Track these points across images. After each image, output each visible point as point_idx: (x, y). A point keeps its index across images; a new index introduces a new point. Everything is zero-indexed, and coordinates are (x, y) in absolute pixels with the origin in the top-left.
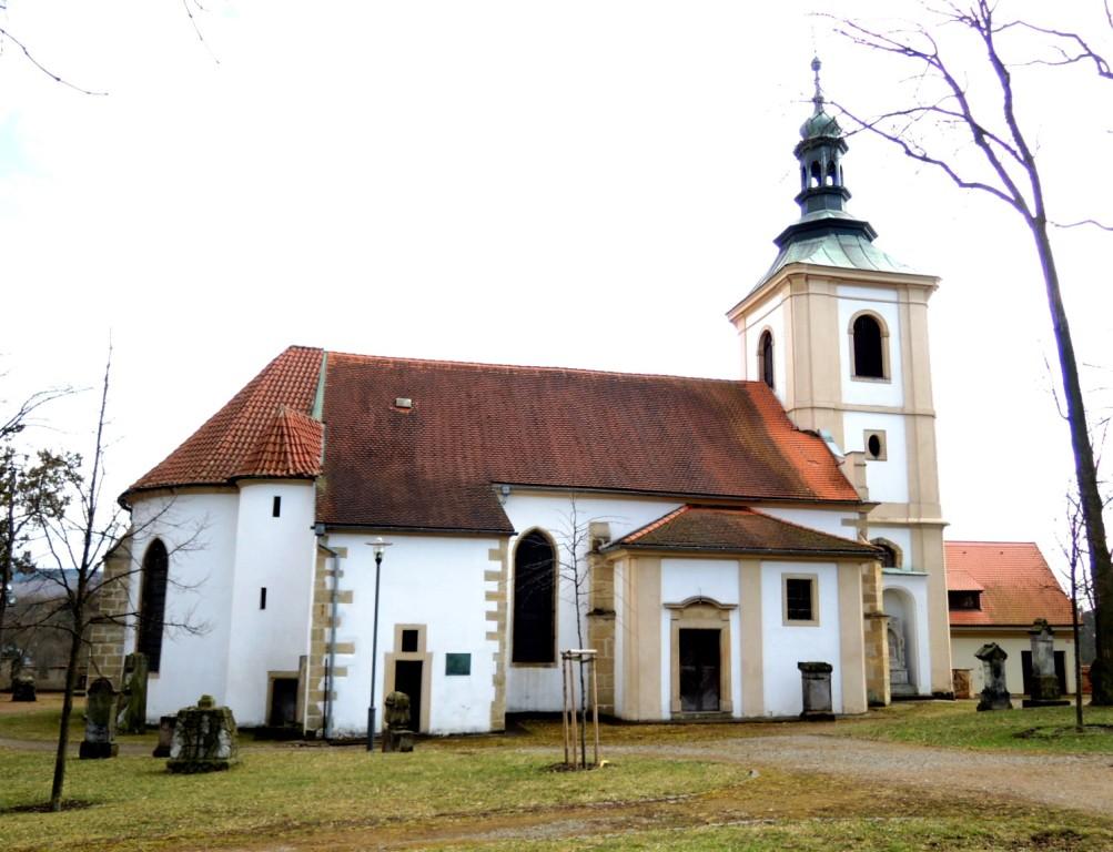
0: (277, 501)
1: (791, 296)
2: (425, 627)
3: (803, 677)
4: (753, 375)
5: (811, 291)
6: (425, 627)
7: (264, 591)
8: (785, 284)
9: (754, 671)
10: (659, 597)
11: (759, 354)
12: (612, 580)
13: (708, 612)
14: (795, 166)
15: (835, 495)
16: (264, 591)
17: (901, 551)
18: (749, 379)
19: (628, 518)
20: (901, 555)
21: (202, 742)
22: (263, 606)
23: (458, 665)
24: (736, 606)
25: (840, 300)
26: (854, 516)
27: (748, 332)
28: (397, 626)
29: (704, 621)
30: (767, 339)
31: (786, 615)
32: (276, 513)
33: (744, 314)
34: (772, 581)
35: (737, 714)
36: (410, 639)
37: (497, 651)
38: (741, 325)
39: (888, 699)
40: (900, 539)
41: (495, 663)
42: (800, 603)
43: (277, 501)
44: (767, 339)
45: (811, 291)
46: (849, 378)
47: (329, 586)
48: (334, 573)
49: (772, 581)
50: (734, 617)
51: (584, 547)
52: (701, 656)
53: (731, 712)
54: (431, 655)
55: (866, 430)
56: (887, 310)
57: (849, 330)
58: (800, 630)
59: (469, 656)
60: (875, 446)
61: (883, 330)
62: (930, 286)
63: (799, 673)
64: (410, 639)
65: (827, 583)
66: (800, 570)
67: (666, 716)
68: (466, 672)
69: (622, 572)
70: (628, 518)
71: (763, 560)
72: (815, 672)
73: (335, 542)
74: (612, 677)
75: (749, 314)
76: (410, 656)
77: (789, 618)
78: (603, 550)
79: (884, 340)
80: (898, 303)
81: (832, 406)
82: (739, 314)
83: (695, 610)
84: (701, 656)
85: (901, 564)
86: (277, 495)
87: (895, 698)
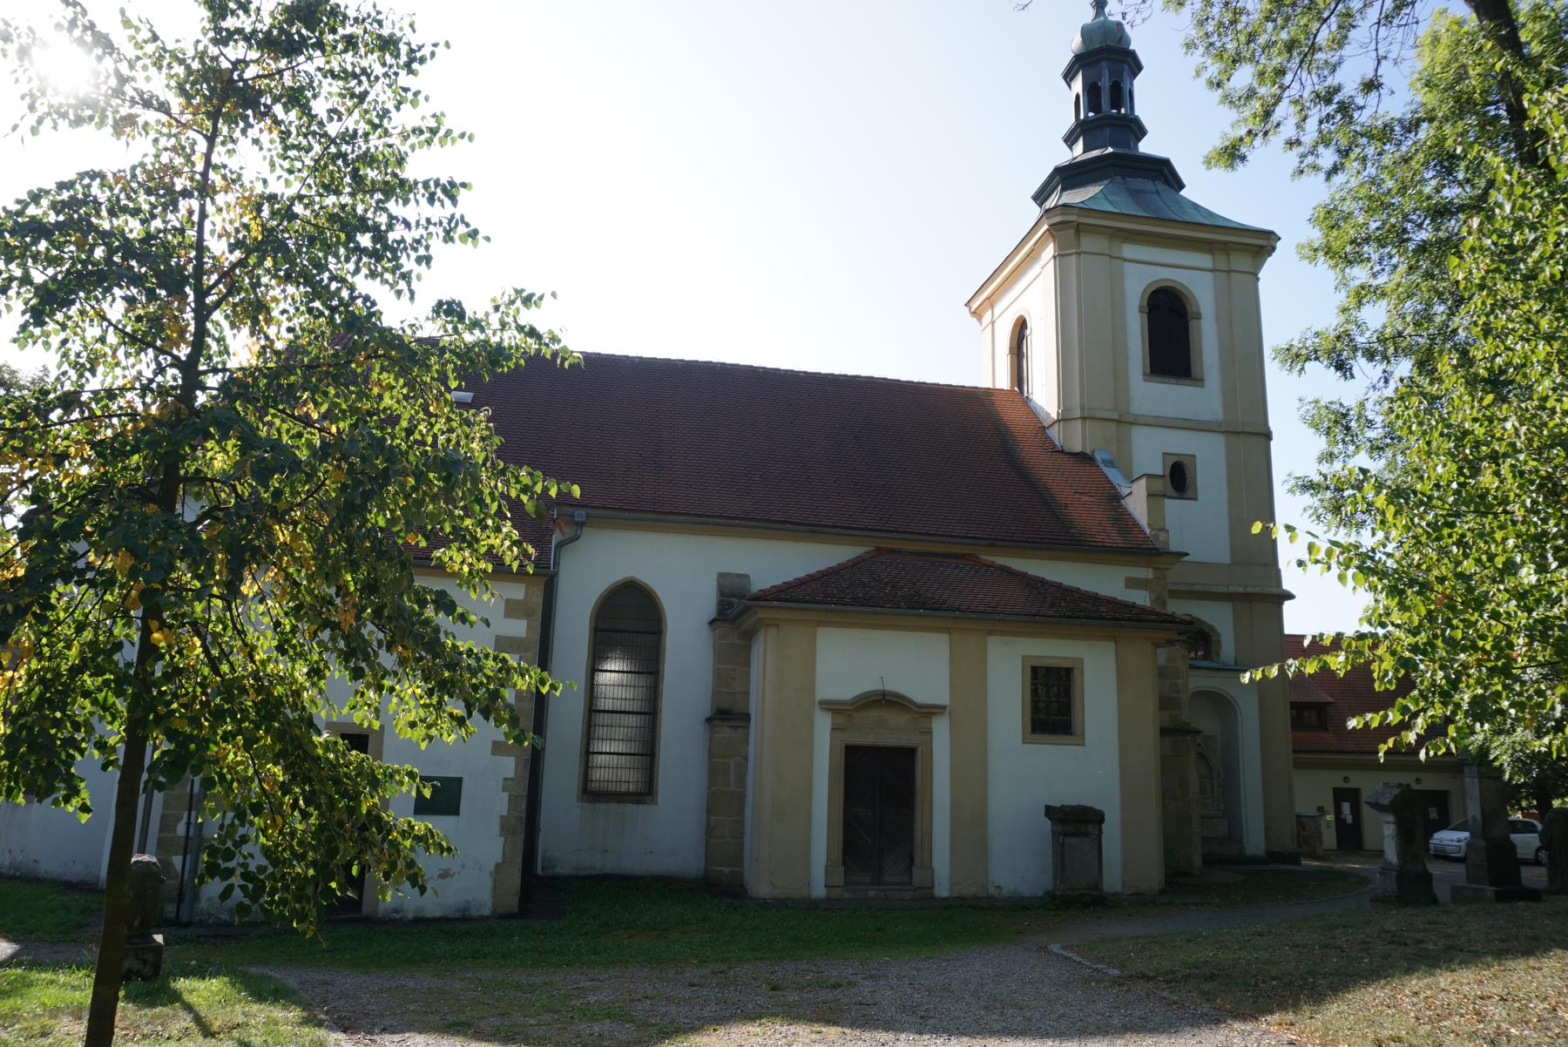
4: (1003, 382)
10: (812, 690)
11: (1011, 352)
12: (748, 664)
13: (895, 718)
15: (1118, 541)
17: (1218, 635)
18: (998, 386)
19: (773, 562)
20: (1218, 642)
23: (444, 797)
24: (944, 707)
29: (889, 732)
30: (1021, 327)
33: (991, 302)
34: (1006, 665)
35: (942, 890)
37: (512, 775)
39: (1198, 862)
40: (1219, 618)
41: (506, 795)
44: (1021, 327)
46: (1141, 376)
49: (1006, 665)
51: (707, 603)
52: (881, 783)
56: (1197, 279)
57: (1141, 307)
58: (1052, 754)
59: (460, 779)
60: (1179, 478)
61: (1191, 310)
62: (1262, 247)
63: (1048, 823)
65: (1101, 676)
66: (1053, 650)
67: (819, 890)
68: (454, 810)
69: (766, 654)
70: (773, 562)
72: (1074, 824)
74: (741, 822)
75: (1000, 298)
77: (1034, 731)
78: (738, 611)
79: (1193, 324)
82: (981, 305)
83: (873, 715)
84: (881, 783)
85: (1218, 655)
87: (1209, 860)
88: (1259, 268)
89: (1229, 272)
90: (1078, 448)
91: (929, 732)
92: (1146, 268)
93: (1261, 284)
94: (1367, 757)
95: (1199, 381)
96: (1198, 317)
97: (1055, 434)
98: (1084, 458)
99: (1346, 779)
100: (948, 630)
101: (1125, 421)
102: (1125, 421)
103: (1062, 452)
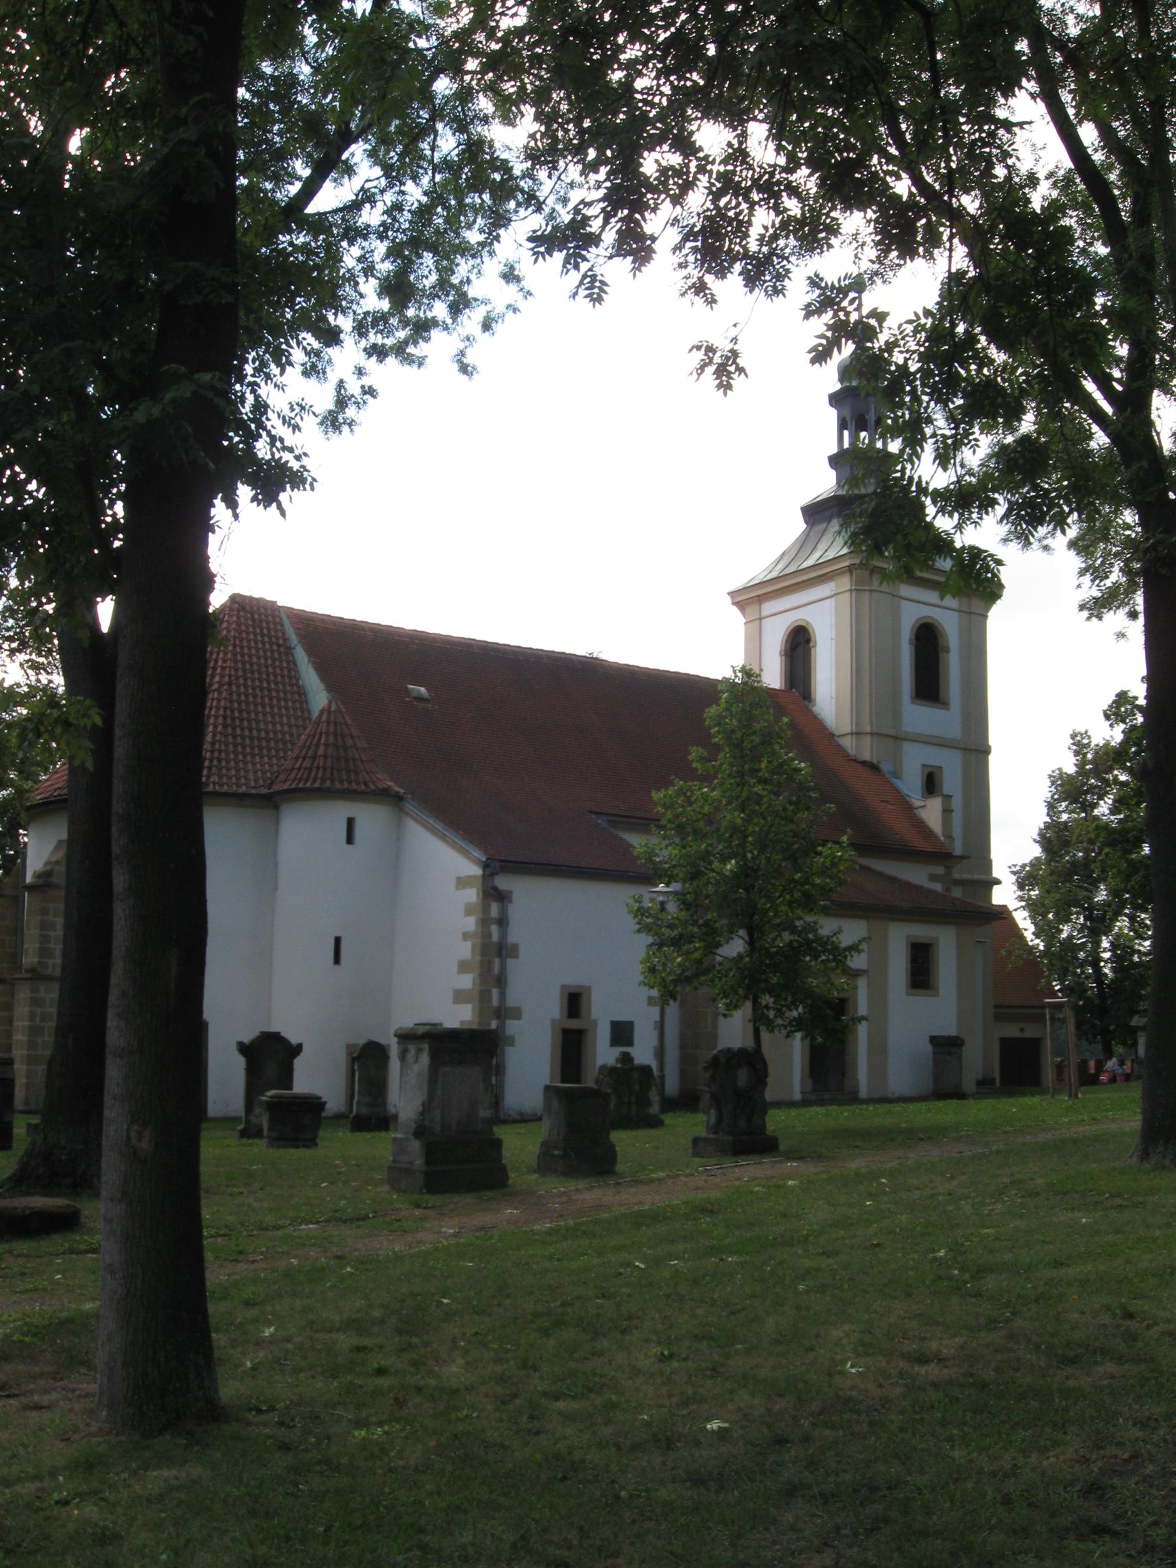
0: (350, 822)
1: (851, 590)
2: (589, 989)
3: (935, 1053)
5: (764, 614)
6: (589, 989)
7: (338, 940)
8: (844, 572)
9: (879, 1049)
14: (831, 416)
16: (338, 940)
21: (633, 1099)
22: (337, 960)
25: (903, 603)
26: (940, 870)
27: (764, 621)
28: (563, 987)
31: (573, 991)
32: (350, 840)
33: (761, 599)
36: (575, 1001)
38: (753, 611)
42: (921, 975)
43: (350, 822)
45: (764, 614)
47: (495, 937)
48: (502, 922)
50: (862, 984)
53: (857, 1092)
54: (595, 1024)
55: (923, 765)
58: (920, 1002)
60: (931, 784)
63: (929, 1048)
64: (575, 1001)
66: (922, 931)
71: (891, 919)
73: (502, 882)
76: (574, 1024)
80: (958, 611)
81: (893, 733)
86: (351, 815)
88: (988, 609)
89: (970, 613)
90: (866, 756)
91: (856, 988)
92: (917, 605)
93: (988, 622)
94: (1038, 1011)
95: (945, 705)
96: (947, 650)
97: (847, 743)
98: (872, 767)
99: (1022, 1030)
100: (867, 918)
101: (899, 738)
102: (899, 738)
103: (855, 761)
